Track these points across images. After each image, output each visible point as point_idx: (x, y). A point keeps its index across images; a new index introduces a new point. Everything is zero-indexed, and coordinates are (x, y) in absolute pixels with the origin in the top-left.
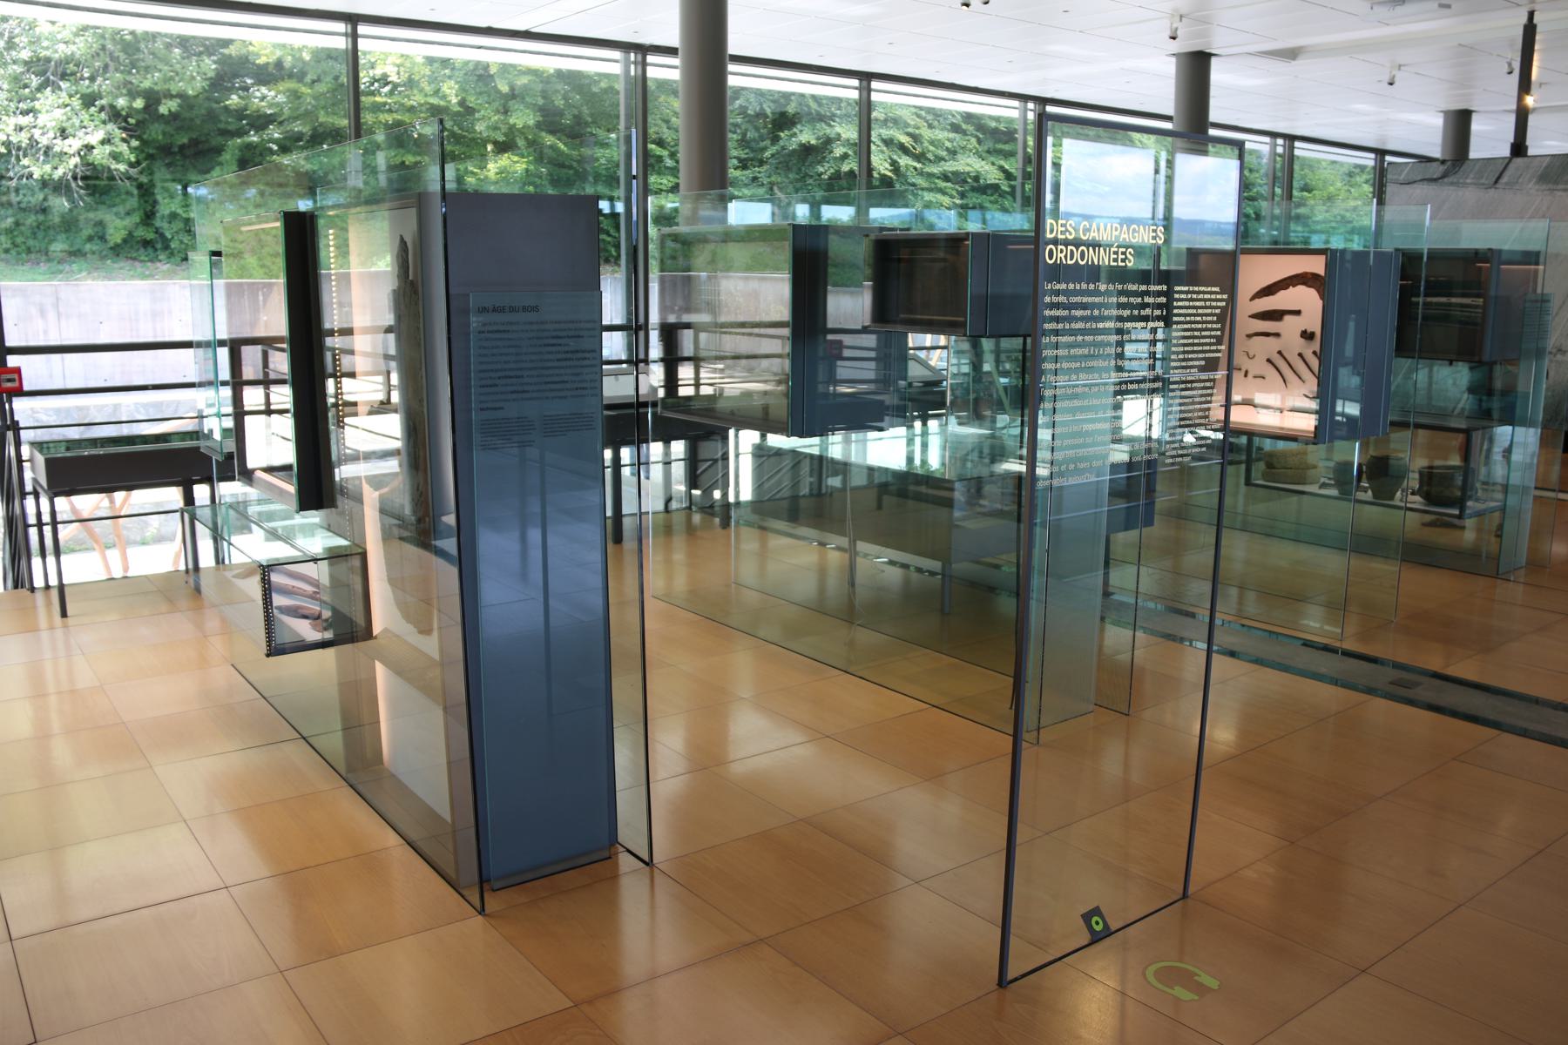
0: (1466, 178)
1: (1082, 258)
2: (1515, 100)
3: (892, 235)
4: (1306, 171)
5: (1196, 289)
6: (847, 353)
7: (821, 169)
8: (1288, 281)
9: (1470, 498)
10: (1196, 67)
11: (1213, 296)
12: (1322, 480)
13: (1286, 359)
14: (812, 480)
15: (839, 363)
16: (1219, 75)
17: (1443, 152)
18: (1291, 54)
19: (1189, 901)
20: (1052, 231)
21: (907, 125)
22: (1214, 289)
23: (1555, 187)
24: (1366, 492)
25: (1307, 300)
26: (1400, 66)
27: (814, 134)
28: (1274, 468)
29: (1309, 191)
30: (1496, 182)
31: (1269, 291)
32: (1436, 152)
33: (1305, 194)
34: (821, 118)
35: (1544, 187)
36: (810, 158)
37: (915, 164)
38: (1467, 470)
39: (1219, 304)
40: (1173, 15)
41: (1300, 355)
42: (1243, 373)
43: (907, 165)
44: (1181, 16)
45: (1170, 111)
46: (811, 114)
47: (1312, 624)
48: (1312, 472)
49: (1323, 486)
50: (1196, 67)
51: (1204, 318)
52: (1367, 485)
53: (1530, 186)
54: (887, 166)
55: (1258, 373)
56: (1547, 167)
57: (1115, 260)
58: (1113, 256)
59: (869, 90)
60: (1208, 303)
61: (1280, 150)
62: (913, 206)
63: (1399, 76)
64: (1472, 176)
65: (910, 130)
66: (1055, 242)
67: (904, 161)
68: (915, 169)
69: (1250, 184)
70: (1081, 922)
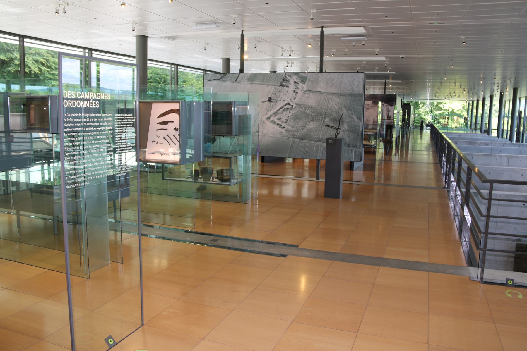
0: (227, 79)
1: (79, 105)
2: (240, 56)
3: (23, 96)
4: (184, 76)
5: (123, 115)
6: (15, 140)
7: (9, 69)
8: (169, 112)
9: (232, 179)
10: (143, 41)
11: (130, 118)
12: (187, 176)
13: (169, 137)
14: (4, 188)
15: (12, 144)
16: (150, 43)
17: (223, 71)
18: (173, 38)
19: (144, 326)
20: (65, 95)
21: (44, 56)
22: (130, 115)
23: (252, 83)
24: (201, 179)
25: (175, 117)
26: (207, 44)
27: (6, 56)
28: (171, 173)
29: (185, 82)
30: (236, 81)
31: (164, 115)
32: (221, 71)
33: (184, 83)
34: (8, 51)
35: (249, 82)
36: (5, 65)
37: (47, 69)
38: (230, 170)
39: (132, 120)
40: (133, 23)
41: (174, 136)
42: (156, 142)
43: (45, 70)
44: (136, 23)
45: (134, 55)
46: (4, 49)
47: (188, 224)
48: (182, 174)
49: (188, 178)
50: (143, 41)
51: (127, 125)
52: (201, 177)
53: (246, 82)
54: (37, 69)
55: (161, 143)
56: (250, 77)
57: (92, 106)
58: (90, 104)
59: (23, 42)
60: (128, 120)
61: (173, 69)
62: (48, 86)
63: (207, 47)
64: (229, 78)
65: (45, 57)
66: (67, 99)
67: (43, 68)
68: (48, 71)
69: (167, 80)
70: (105, 342)
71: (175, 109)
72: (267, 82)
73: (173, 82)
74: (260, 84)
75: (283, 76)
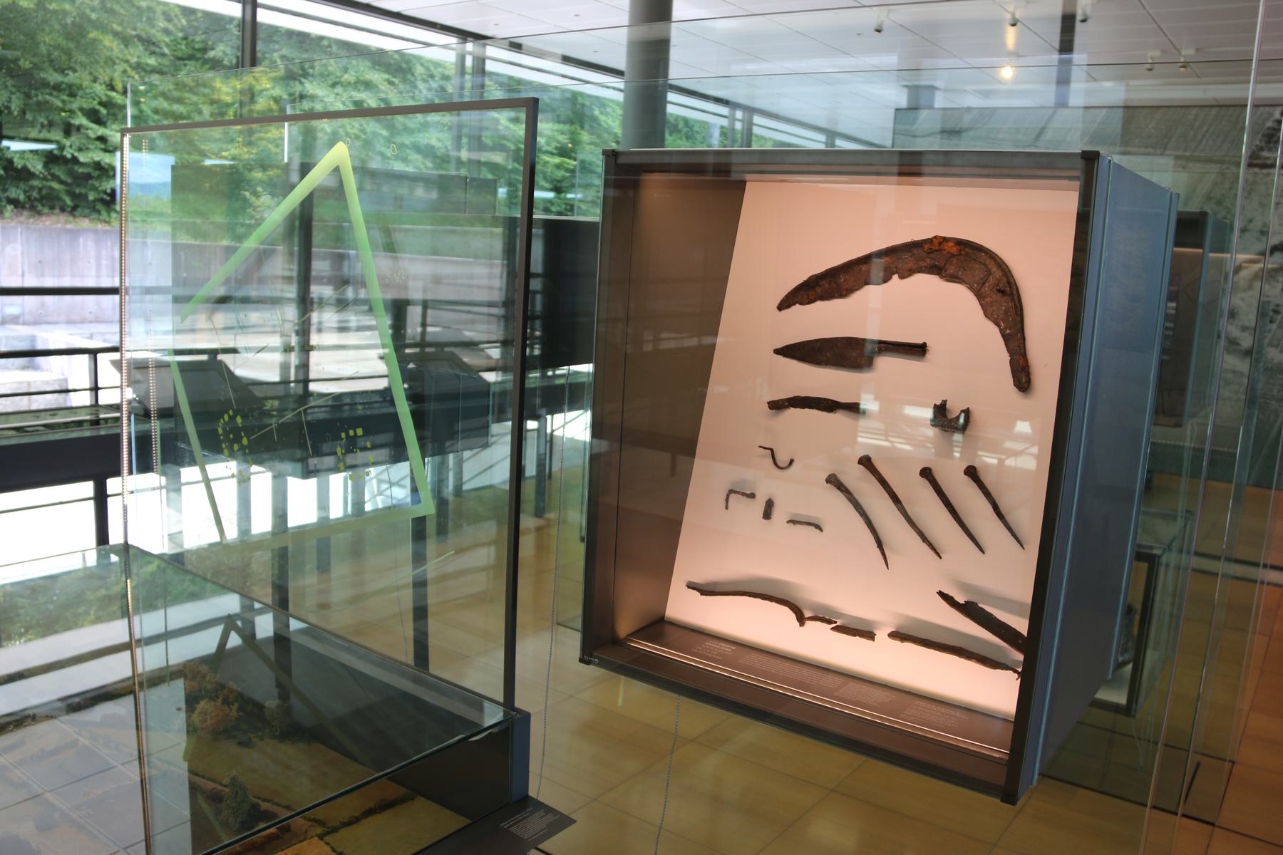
41: (926, 473)
71: (945, 239)
72: (1186, 150)
73: (428, 350)
74: (1148, 154)
75: (1267, 120)
